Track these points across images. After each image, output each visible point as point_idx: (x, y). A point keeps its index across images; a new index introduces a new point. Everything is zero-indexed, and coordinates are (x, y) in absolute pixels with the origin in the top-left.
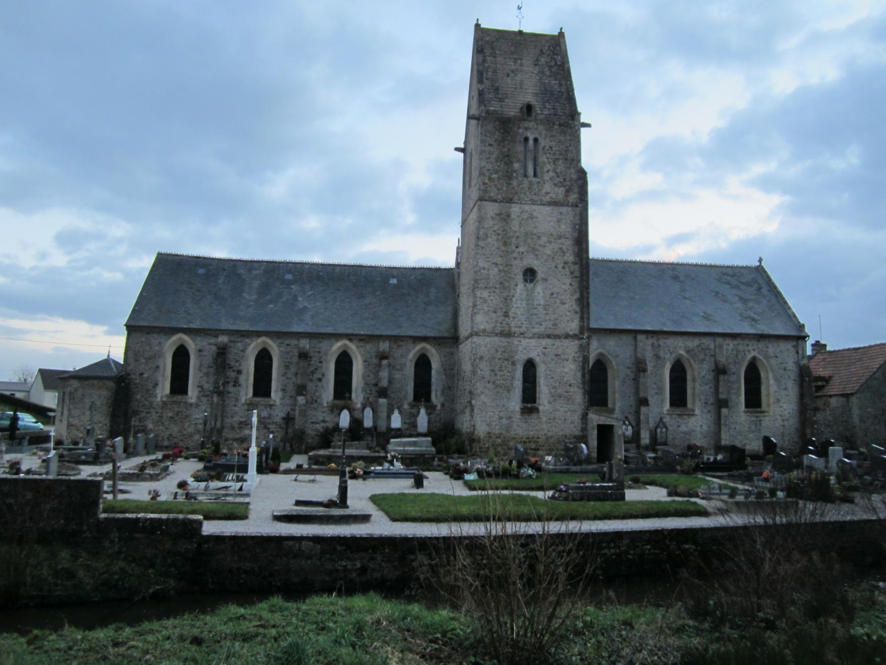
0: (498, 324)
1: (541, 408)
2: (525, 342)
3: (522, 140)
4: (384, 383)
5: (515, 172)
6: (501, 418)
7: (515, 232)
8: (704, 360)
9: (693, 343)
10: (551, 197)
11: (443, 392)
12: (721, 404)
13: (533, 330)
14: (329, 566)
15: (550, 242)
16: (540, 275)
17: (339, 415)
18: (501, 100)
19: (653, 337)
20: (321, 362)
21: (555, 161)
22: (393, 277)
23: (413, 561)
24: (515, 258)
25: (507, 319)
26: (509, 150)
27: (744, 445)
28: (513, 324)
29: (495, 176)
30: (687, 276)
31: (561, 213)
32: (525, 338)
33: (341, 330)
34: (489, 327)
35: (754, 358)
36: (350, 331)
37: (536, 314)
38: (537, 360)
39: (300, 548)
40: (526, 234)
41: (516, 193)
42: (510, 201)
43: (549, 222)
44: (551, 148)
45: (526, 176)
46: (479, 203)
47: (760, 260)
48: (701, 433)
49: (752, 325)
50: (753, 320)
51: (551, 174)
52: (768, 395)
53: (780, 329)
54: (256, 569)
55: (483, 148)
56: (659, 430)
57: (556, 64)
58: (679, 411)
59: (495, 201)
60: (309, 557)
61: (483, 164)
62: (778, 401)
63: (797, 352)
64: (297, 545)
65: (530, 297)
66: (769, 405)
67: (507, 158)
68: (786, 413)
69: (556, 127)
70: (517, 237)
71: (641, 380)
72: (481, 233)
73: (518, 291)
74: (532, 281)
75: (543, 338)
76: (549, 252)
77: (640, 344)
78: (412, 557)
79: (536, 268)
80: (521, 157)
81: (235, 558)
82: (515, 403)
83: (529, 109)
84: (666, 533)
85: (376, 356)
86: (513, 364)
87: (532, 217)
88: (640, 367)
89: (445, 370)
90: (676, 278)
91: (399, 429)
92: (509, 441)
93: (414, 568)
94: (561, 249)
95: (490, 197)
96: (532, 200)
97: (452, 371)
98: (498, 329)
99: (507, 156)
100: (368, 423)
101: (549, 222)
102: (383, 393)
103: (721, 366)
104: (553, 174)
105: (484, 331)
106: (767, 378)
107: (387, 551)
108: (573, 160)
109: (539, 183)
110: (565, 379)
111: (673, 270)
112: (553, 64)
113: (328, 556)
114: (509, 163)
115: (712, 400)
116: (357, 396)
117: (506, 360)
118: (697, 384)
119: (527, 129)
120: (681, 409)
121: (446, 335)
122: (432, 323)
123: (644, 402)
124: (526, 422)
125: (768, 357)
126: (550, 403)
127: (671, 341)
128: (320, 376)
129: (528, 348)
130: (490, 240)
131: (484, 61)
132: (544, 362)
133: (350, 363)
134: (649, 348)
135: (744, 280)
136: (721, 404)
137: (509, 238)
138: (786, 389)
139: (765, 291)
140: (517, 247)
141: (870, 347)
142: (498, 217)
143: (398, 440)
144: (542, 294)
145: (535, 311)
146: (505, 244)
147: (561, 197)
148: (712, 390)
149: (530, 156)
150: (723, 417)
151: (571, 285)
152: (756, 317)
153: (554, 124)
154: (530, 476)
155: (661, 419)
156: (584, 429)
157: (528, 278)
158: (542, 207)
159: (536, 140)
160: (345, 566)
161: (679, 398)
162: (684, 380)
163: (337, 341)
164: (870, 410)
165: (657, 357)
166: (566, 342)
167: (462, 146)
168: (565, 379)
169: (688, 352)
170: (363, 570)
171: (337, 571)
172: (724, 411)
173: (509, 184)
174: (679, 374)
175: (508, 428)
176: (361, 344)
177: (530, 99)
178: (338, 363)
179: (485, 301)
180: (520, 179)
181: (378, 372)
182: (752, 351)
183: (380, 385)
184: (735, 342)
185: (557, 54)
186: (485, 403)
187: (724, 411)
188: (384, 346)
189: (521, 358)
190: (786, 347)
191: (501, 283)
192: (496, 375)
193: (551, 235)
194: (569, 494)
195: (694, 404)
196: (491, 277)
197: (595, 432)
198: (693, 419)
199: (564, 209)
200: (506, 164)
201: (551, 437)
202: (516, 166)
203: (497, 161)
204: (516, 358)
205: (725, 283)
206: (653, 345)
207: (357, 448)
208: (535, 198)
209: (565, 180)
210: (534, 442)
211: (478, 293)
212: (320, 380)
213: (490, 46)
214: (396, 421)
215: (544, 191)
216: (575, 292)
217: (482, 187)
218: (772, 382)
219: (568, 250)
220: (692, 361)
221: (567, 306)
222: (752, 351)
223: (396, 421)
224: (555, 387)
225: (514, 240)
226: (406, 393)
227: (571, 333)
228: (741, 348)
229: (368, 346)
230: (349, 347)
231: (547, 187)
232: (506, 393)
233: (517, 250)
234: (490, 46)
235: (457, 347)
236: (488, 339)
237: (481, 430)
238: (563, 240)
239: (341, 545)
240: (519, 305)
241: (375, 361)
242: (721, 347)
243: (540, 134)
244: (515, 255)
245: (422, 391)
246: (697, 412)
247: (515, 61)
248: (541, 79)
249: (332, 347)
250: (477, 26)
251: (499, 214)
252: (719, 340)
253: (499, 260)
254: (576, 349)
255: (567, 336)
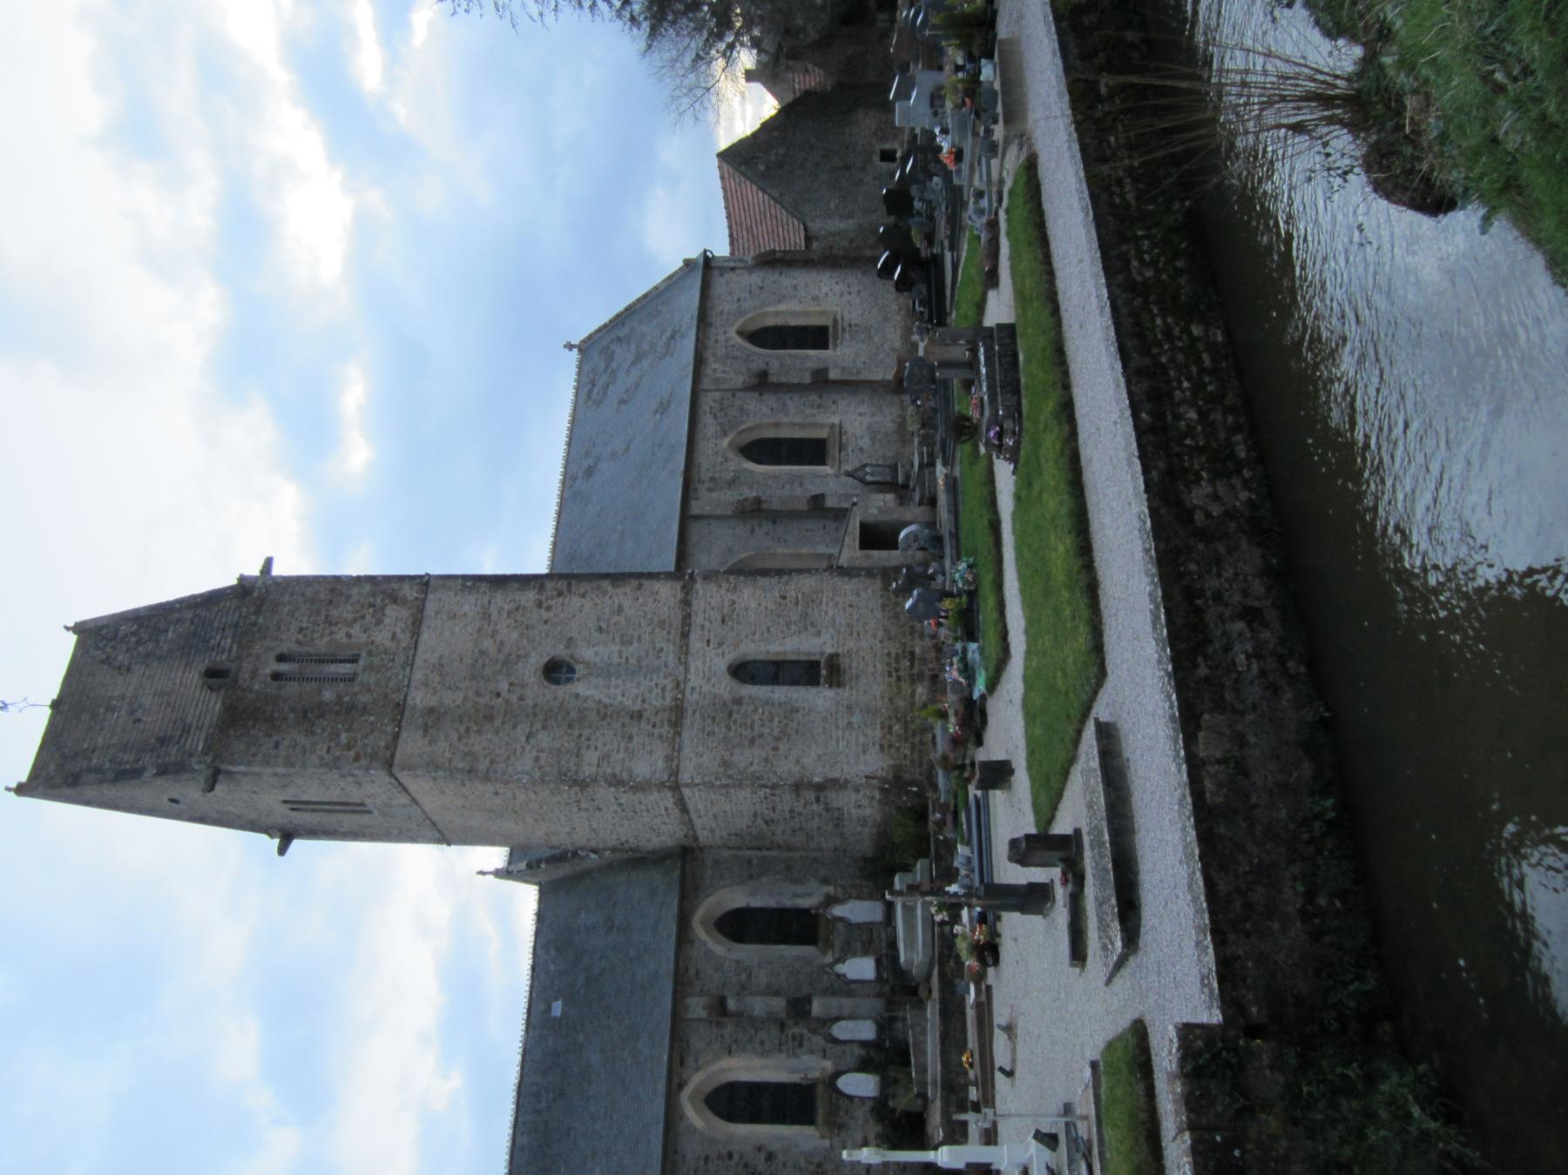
0: (656, 731)
1: (829, 650)
2: (694, 680)
3: (276, 684)
4: (779, 1004)
5: (340, 698)
6: (850, 724)
7: (465, 698)
8: (742, 409)
9: (709, 425)
10: (403, 631)
11: (797, 881)
12: (821, 382)
13: (671, 665)
14: (1254, 693)
15: (495, 632)
16: (560, 652)
17: (851, 1098)
18: (186, 730)
19: (696, 490)
20: (730, 1156)
21: (329, 621)
22: (549, 1009)
23: (1208, 515)
24: (521, 698)
25: (646, 715)
26: (293, 710)
27: (894, 350)
28: (658, 703)
29: (344, 738)
30: (587, 454)
31: (437, 613)
32: (686, 680)
33: (659, 1106)
34: (661, 750)
35: (740, 333)
36: (661, 1086)
37: (639, 659)
38: (731, 657)
39: (1219, 762)
40: (473, 677)
41: (386, 695)
42: (400, 708)
43: (452, 634)
44: (301, 630)
45: (351, 679)
46: (395, 770)
47: (570, 347)
48: (874, 415)
49: (682, 336)
50: (673, 337)
51: (356, 630)
52: (805, 314)
53: (690, 298)
54: (1296, 869)
55: (281, 760)
56: (869, 478)
57: (133, 634)
58: (833, 450)
59: (396, 737)
60: (1240, 740)
61: (314, 759)
62: (815, 298)
63: (733, 269)
64: (1212, 769)
65: (606, 671)
66: (823, 313)
67: (309, 715)
68: (837, 288)
69: (261, 620)
70: (478, 694)
71: (776, 506)
72: (461, 765)
73: (588, 693)
74: (572, 671)
75: (687, 645)
76: (515, 635)
77: (707, 510)
78: (1199, 516)
79: (546, 659)
80: (310, 687)
81: (1276, 926)
82: (820, 698)
83: (214, 675)
84: (1080, 117)
85: (719, 1024)
86: (738, 701)
87: (439, 667)
88: (753, 511)
89: (750, 877)
90: (590, 472)
91: (878, 963)
92: (897, 710)
93: (1226, 513)
94: (509, 613)
95: (387, 748)
96: (403, 667)
97: (757, 853)
98: (666, 730)
99: (305, 712)
100: (866, 1030)
101: (452, 634)
102: (799, 1008)
103: (754, 380)
104: (357, 626)
105: (668, 759)
106: (777, 314)
107: (1193, 567)
108: (332, 591)
109: (370, 653)
110: (771, 606)
111: (575, 478)
112: (133, 639)
113: (1228, 696)
114: (321, 710)
115: (814, 397)
116: (806, 1066)
117: (730, 715)
118: (785, 420)
119: (254, 674)
120: (829, 447)
121: (676, 874)
122: (650, 907)
123: (817, 502)
124: (858, 677)
125: (740, 313)
126: (818, 634)
127: (705, 460)
128: (762, 1156)
129: (707, 671)
130: (477, 748)
131: (99, 770)
132: (737, 645)
133: (732, 1087)
134: (715, 495)
135: (602, 365)
136: (821, 382)
137: (477, 711)
138: (795, 287)
139: (622, 333)
140: (498, 695)
141: (729, 217)
142: (431, 731)
143: (901, 946)
144: (600, 649)
145: (632, 661)
146: (489, 718)
147: (405, 613)
148: (796, 397)
149: (312, 669)
150: (845, 377)
151: (583, 596)
152: (668, 334)
153: (255, 624)
154: (970, 567)
155: (848, 474)
156: (870, 573)
157: (563, 676)
158: (421, 647)
159: (281, 658)
160: (1248, 657)
161: (812, 451)
162: (778, 442)
163: (682, 1116)
164: (832, 206)
165: (732, 483)
166: (698, 604)
167: (277, 841)
168: (771, 606)
169: (725, 434)
170: (1250, 614)
171: (1263, 673)
172: (833, 375)
173: (365, 710)
174: (764, 450)
175: (869, 711)
176: (690, 1061)
177: (194, 677)
178: (731, 1116)
179: (606, 757)
180: (357, 689)
181: (752, 1020)
182: (727, 335)
183: (783, 1015)
184: (711, 360)
185: (116, 632)
186: (819, 757)
187: (833, 375)
188: (697, 1007)
189: (726, 687)
190: (720, 284)
191: (570, 726)
192: (761, 736)
193: (480, 630)
194: (1005, 417)
195: (823, 425)
196: (556, 745)
197: (875, 553)
198: (848, 426)
199: (431, 607)
200: (322, 716)
201: (886, 631)
202: (328, 695)
203: (313, 733)
204: (727, 697)
205: (605, 393)
206: (709, 490)
207: (924, 1031)
208: (400, 660)
209: (372, 605)
210: (897, 662)
211: (588, 771)
212: (770, 1157)
213: (76, 762)
214: (861, 968)
215: (388, 644)
216: (599, 588)
217: (363, 763)
218: (782, 307)
219: (513, 600)
220: (743, 427)
221: (626, 603)
222: (727, 335)
223: (861, 968)
224: (788, 625)
225: (482, 701)
226: (799, 958)
227: (680, 596)
228: (721, 351)
229: (696, 1044)
230: (697, 1090)
231: (382, 637)
232: (799, 716)
233: (504, 694)
234: (76, 762)
235: (702, 849)
236: (686, 751)
237: (875, 763)
238: (493, 610)
239: (1196, 666)
240: (619, 692)
241: (729, 1029)
242: (717, 380)
243: (269, 649)
244: (514, 698)
245: (798, 927)
246: (836, 420)
247: (111, 709)
248: (160, 658)
249: (695, 1130)
250: (21, 790)
251: (426, 728)
252: (706, 383)
253: (521, 731)
254: (713, 587)
255: (686, 602)
